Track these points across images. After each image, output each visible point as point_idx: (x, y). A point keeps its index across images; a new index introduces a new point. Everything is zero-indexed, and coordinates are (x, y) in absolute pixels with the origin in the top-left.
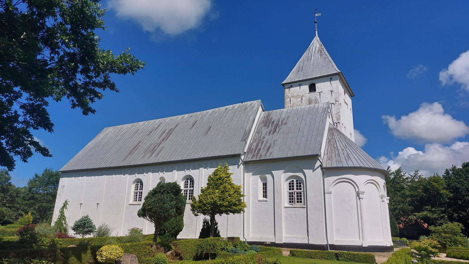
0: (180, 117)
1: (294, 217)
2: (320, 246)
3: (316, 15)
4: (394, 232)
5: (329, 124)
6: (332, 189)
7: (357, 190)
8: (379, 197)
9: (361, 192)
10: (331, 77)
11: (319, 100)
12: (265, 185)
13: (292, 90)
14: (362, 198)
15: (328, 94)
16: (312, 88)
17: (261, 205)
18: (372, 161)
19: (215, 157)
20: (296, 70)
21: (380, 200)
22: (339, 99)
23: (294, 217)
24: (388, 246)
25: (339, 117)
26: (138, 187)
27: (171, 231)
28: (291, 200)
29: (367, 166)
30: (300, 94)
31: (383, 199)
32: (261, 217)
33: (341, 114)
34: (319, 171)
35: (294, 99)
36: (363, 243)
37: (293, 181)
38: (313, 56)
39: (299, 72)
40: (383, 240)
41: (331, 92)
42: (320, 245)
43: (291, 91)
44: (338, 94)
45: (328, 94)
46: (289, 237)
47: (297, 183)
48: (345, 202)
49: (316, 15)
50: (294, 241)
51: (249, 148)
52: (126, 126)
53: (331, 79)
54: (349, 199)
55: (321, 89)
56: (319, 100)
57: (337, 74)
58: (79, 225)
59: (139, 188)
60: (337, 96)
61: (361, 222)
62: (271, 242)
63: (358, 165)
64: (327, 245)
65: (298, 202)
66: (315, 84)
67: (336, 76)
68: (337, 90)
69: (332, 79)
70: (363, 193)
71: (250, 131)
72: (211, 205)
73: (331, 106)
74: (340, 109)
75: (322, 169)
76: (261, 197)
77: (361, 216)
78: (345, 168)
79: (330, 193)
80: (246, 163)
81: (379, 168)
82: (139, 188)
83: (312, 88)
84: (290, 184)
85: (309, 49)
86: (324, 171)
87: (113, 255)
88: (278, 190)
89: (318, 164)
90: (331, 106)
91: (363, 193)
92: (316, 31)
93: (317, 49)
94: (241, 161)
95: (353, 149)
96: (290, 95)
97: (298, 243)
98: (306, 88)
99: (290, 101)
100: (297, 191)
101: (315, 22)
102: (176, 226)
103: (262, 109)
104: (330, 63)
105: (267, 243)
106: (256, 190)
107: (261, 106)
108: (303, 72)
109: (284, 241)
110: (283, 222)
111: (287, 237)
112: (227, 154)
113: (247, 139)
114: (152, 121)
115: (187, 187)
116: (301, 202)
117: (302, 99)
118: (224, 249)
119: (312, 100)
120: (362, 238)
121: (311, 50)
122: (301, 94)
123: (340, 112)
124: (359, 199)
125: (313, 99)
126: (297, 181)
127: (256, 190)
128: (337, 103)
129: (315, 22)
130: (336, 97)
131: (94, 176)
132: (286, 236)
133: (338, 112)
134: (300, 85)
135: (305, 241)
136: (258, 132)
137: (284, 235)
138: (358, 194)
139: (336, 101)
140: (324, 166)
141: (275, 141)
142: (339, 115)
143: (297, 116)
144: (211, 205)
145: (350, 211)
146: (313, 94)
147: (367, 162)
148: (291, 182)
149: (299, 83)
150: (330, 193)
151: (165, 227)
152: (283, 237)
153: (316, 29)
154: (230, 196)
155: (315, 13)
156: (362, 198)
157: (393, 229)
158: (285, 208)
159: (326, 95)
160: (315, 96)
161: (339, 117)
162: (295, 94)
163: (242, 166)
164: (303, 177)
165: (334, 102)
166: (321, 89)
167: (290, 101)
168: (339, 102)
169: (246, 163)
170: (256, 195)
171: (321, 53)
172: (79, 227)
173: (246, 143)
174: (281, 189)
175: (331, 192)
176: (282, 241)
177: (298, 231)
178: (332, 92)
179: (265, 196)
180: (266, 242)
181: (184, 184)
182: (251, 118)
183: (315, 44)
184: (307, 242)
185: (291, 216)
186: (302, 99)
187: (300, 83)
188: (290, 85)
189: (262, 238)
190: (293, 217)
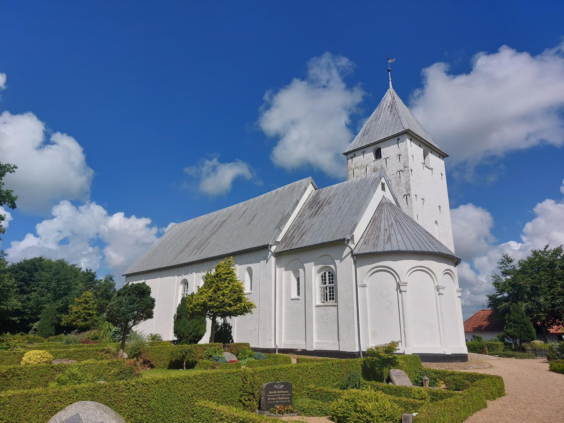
0: (235, 206)
1: (325, 317)
2: (351, 354)
3: (390, 61)
4: (528, 336)
5: (382, 198)
6: (367, 281)
7: (398, 281)
8: (435, 289)
9: (403, 283)
10: (398, 137)
11: (385, 168)
12: (298, 279)
13: (355, 160)
14: (405, 291)
15: (396, 159)
16: (378, 155)
17: (294, 304)
18: (423, 241)
19: (258, 248)
20: (362, 134)
21: (436, 292)
22: (408, 164)
23: (325, 317)
24: (446, 354)
25: (409, 188)
26: (325, 280)
27: (188, 337)
28: (331, 297)
29: (431, 250)
30: (363, 164)
31: (440, 292)
32: (294, 319)
33: (412, 183)
34: (350, 259)
35: (357, 170)
36: (405, 350)
37: (325, 273)
38: (382, 114)
39: (364, 136)
40: (439, 346)
41: (398, 156)
42: (350, 352)
43: (354, 161)
44: (406, 158)
45: (396, 159)
46: (321, 343)
47: (329, 276)
48: (384, 297)
49: (390, 61)
50: (325, 347)
51: (285, 237)
52: (190, 221)
53: (398, 139)
54: (387, 293)
55: (387, 154)
56: (385, 168)
57: (404, 133)
58: (116, 332)
59: (327, 281)
60: (406, 161)
61: (404, 322)
62: (302, 350)
63: (412, 249)
64: (359, 352)
65: (330, 299)
66: (380, 149)
67: (404, 135)
68: (405, 153)
69: (399, 140)
70: (405, 284)
71: (289, 215)
72: (201, 306)
73: (400, 174)
74: (409, 177)
75: (353, 256)
76: (294, 295)
77: (403, 315)
78: (379, 253)
79: (365, 286)
80: (278, 255)
81: (441, 252)
82: (327, 281)
83: (378, 155)
84: (322, 277)
85: (380, 106)
86: (355, 259)
87: (32, 360)
88: (309, 286)
89: (347, 250)
90: (400, 174)
91: (405, 284)
92: (390, 81)
93: (388, 104)
94: (270, 253)
95: (400, 228)
96: (353, 166)
97: (328, 351)
98: (370, 155)
99: (353, 173)
100: (330, 285)
101: (389, 71)
102: (193, 331)
103: (314, 187)
104: (399, 119)
105: (298, 351)
106: (288, 287)
107: (312, 184)
108: (368, 136)
109: (315, 347)
110: (235, 326)
111: (319, 343)
112: (260, 245)
113: (283, 226)
114: (211, 214)
115: (325, 283)
116: (333, 299)
117: (366, 170)
118: (210, 356)
119: (377, 168)
120: (405, 344)
121: (381, 106)
122: (365, 164)
123: (410, 180)
124: (401, 292)
125: (379, 167)
126: (329, 273)
127: (288, 287)
128: (405, 169)
129: (389, 71)
130: (404, 162)
131: (166, 277)
132: (318, 341)
133: (408, 181)
134: (364, 153)
135: (335, 348)
136: (300, 215)
137: (315, 340)
138: (438, 288)
139: (405, 167)
140: (355, 252)
141: (312, 225)
142: (409, 185)
143: (345, 192)
144: (201, 306)
145: (389, 309)
146: (378, 161)
147: (431, 245)
148: (323, 274)
149: (362, 150)
150: (365, 286)
151: (181, 333)
152: (314, 344)
153: (390, 79)
154: (223, 295)
155: (388, 59)
156: (405, 291)
157: (525, 333)
158: (317, 306)
159: (393, 161)
160: (380, 164)
161: (409, 188)
162: (359, 165)
163: (273, 259)
164: (334, 268)
165: (402, 168)
166: (387, 154)
167: (353, 173)
168: (408, 168)
169: (278, 255)
170: (288, 293)
171: (392, 108)
172: (117, 334)
173: (280, 231)
174: (312, 284)
175: (407, 283)
176: (312, 348)
177: (330, 335)
178: (400, 156)
179: (299, 294)
180: (297, 349)
181: (321, 280)
182: (295, 200)
183: (387, 98)
184: (338, 349)
185: (322, 317)
186: (366, 170)
187: (363, 150)
188: (352, 155)
189: (294, 345)
190: (325, 318)
